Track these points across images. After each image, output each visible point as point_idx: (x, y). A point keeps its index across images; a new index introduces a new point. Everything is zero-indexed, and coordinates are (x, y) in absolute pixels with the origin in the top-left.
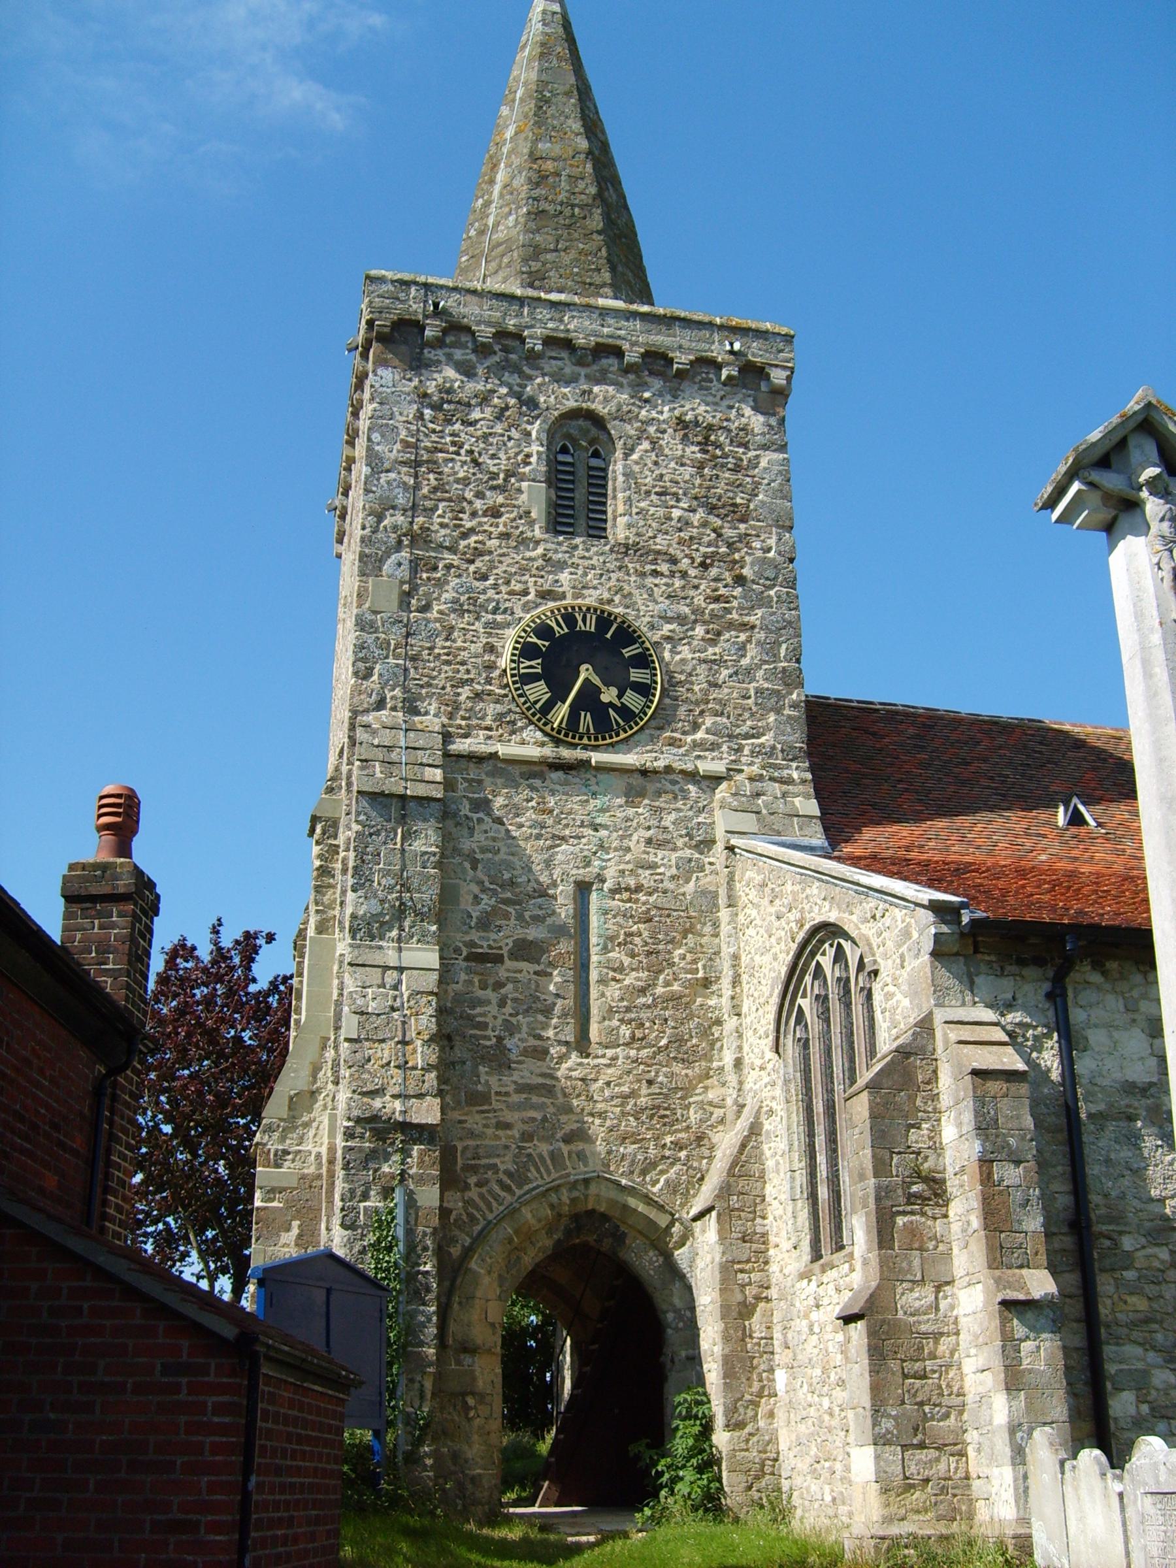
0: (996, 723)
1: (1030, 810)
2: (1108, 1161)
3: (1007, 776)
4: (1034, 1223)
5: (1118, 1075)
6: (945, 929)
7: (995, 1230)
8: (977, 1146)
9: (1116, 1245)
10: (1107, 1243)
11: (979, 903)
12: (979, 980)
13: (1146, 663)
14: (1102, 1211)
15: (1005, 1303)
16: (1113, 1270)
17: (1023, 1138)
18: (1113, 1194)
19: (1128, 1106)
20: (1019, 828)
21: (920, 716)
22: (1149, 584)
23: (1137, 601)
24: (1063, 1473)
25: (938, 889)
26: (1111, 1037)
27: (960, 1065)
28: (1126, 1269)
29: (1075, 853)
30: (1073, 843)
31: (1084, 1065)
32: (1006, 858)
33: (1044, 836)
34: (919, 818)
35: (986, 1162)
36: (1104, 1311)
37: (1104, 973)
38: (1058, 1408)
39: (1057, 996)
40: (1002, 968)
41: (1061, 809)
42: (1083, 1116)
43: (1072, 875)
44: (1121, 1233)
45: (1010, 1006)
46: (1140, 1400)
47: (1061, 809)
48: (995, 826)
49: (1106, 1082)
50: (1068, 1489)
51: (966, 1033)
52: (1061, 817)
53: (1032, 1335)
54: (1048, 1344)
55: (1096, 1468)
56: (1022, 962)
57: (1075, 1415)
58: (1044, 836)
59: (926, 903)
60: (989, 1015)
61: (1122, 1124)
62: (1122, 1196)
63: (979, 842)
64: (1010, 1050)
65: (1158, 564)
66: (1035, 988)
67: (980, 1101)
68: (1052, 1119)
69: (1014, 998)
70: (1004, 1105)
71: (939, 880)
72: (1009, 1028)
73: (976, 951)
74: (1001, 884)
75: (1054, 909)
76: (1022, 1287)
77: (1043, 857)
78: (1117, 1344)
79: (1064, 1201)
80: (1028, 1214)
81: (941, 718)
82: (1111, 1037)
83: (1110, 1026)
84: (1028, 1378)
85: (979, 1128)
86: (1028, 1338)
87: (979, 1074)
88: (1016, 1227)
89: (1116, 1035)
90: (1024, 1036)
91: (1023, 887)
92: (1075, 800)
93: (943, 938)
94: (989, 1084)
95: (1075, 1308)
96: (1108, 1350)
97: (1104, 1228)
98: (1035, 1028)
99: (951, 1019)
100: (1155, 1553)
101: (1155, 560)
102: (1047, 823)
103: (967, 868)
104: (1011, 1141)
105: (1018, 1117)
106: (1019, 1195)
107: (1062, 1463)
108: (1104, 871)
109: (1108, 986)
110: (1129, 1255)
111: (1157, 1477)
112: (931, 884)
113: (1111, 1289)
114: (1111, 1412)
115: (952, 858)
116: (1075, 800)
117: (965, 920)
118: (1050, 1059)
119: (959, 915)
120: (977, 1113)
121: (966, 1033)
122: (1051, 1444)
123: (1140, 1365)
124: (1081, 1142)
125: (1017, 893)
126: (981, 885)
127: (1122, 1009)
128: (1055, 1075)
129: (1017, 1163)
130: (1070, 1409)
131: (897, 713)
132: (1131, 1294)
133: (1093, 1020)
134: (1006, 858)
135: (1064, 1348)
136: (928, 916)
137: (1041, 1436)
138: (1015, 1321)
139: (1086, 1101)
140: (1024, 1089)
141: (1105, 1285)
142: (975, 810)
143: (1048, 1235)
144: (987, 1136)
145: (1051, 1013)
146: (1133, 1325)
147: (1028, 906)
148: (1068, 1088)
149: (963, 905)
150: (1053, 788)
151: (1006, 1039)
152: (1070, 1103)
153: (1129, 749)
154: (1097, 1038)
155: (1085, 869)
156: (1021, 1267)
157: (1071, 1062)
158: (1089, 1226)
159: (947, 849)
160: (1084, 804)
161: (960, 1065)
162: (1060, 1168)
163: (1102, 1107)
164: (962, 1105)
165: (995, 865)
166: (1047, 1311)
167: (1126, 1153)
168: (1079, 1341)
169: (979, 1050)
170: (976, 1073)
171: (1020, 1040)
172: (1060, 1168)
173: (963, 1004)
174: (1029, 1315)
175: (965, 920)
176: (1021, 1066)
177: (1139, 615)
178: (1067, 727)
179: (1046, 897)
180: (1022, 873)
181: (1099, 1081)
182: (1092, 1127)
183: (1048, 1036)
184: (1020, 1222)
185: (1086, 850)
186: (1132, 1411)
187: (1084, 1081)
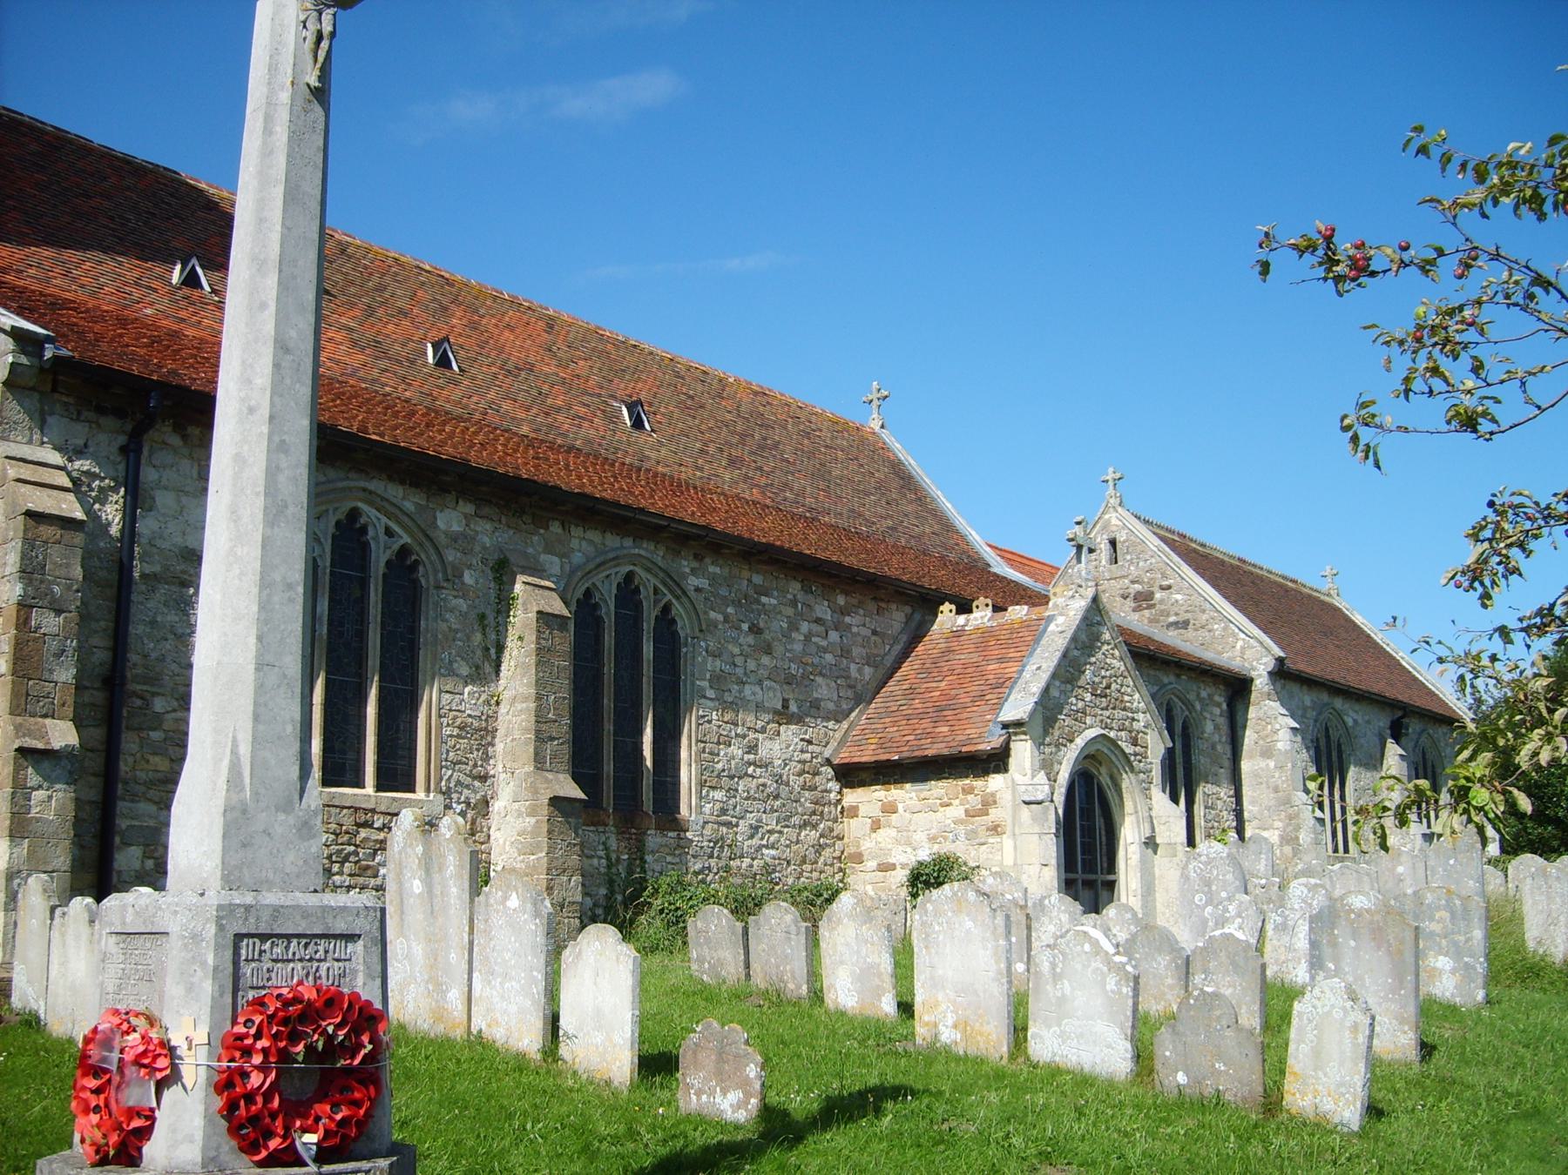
0: (129, 163)
1: (146, 261)
2: (153, 623)
3: (129, 220)
4: (65, 674)
5: (179, 540)
6: (24, 360)
7: (23, 677)
8: (18, 589)
9: (148, 705)
10: (139, 702)
11: (68, 341)
12: (50, 420)
13: (268, 119)
14: (139, 671)
15: (22, 751)
16: (140, 729)
17: (69, 588)
18: (154, 655)
19: (184, 572)
20: (132, 275)
21: (47, 133)
22: (290, 38)
23: (275, 53)
24: (52, 919)
25: (27, 319)
26: (179, 501)
27: (14, 504)
28: (154, 729)
29: (183, 314)
30: (183, 304)
31: (145, 526)
32: (110, 303)
33: (155, 290)
34: (23, 241)
35: (24, 607)
36: (124, 768)
37: (185, 437)
38: (61, 858)
39: (131, 452)
40: (79, 413)
41: (178, 267)
42: (136, 575)
43: (175, 335)
44: (154, 694)
45: (79, 453)
46: (146, 856)
47: (178, 267)
48: (104, 268)
49: (165, 545)
50: (55, 934)
51: (27, 472)
52: (176, 276)
53: (45, 785)
54: (60, 794)
55: (86, 915)
56: (101, 410)
57: (77, 866)
58: (155, 290)
59: (8, 328)
60: (56, 458)
61: (174, 588)
62: (162, 659)
63: (84, 280)
64: (71, 497)
65: (304, 22)
66: (110, 439)
67: (29, 543)
68: (103, 574)
69: (86, 445)
70: (55, 554)
71: (31, 311)
72: (75, 474)
73: (54, 390)
74: (97, 328)
75: (146, 363)
76: (43, 736)
77: (149, 311)
78: (132, 801)
79: (101, 656)
80: (61, 665)
81: (71, 142)
82: (179, 501)
83: (180, 491)
84: (34, 826)
85: (23, 571)
86: (40, 787)
87: (32, 516)
88: (46, 676)
89: (184, 499)
90: (89, 485)
91: (121, 336)
92: (194, 261)
93: (20, 369)
94: (42, 528)
95: (96, 762)
96: (122, 806)
97: (139, 687)
98: (102, 479)
99: (12, 454)
100: (110, 989)
101: (302, 18)
102: (161, 278)
103: (66, 304)
104: (56, 589)
105: (68, 566)
106: (54, 645)
107: (53, 909)
108: (210, 339)
109: (185, 451)
110: (159, 717)
111: (124, 917)
112: (20, 312)
113: (134, 747)
114: (116, 866)
115: (51, 290)
116: (194, 261)
117: (48, 354)
118: (112, 513)
119: (43, 349)
120: (24, 556)
121: (27, 472)
122: (45, 891)
123: (152, 823)
124: (128, 601)
125: (112, 341)
126: (75, 324)
127: (195, 475)
128: (114, 530)
129: (59, 612)
130: (73, 860)
131: (22, 123)
132: (155, 754)
133: (164, 481)
134: (110, 303)
135: (77, 799)
136: (4, 343)
137: (36, 882)
138: (30, 770)
139: (142, 560)
140: (79, 538)
141: (130, 743)
142: (85, 247)
143: (79, 688)
144: (31, 580)
145: (122, 467)
146: (150, 784)
147: (120, 356)
148: (126, 546)
149: (48, 339)
150: (175, 244)
151: (70, 485)
152: (125, 560)
153: (233, 206)
154: (164, 500)
155: (190, 332)
156: (45, 716)
157: (133, 520)
158: (123, 684)
159: (48, 280)
160: (203, 267)
161: (14, 504)
162: (103, 624)
163: (157, 568)
164: (10, 545)
165: (97, 308)
166: (64, 762)
167: (172, 617)
168: (93, 795)
169: (38, 491)
170: (29, 514)
171: (84, 488)
172: (103, 624)
173: (30, 442)
174: (46, 765)
175: (48, 354)
176: (79, 514)
177: (273, 68)
178: (203, 186)
179: (142, 352)
180: (123, 322)
181: (159, 543)
182: (143, 587)
183: (115, 490)
184: (51, 671)
185: (195, 314)
186: (137, 865)
187: (144, 541)
